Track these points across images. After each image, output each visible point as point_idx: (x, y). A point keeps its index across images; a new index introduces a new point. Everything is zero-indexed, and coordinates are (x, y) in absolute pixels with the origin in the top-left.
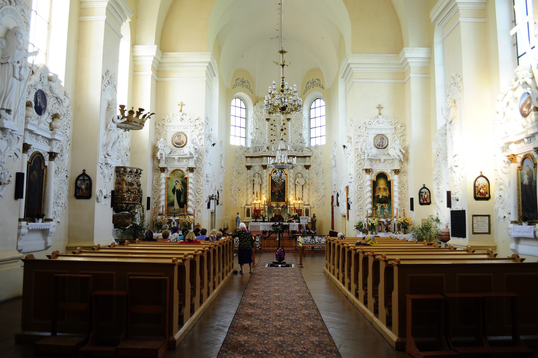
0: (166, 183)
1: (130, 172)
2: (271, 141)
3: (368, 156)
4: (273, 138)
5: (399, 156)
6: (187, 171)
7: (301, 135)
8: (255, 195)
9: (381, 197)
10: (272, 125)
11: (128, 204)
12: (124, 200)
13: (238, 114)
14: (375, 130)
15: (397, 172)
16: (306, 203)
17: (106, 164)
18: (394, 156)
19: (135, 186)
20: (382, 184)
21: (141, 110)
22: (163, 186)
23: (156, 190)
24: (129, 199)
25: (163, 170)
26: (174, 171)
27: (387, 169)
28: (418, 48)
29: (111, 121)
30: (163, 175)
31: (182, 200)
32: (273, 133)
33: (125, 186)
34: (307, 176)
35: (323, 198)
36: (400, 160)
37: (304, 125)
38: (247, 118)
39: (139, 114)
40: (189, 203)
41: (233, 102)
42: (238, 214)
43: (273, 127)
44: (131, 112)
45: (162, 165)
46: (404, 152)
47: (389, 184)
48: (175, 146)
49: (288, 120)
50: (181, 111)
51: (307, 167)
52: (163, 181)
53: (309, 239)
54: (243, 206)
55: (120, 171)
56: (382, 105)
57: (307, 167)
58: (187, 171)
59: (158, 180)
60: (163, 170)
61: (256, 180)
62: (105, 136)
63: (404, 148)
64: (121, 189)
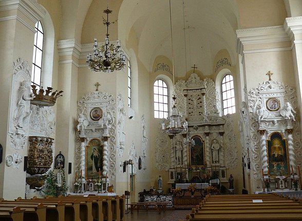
0: (86, 150)
1: (41, 140)
2: (190, 113)
3: (261, 118)
4: (191, 111)
5: (290, 116)
6: (102, 140)
7: (215, 106)
8: (178, 160)
9: (276, 156)
10: (189, 99)
11: (39, 168)
12: (35, 165)
13: (161, 93)
14: (267, 94)
15: (289, 132)
16: (222, 166)
17: (17, 134)
18: (286, 117)
19: (46, 152)
20: (277, 143)
21: (49, 89)
22: (84, 153)
23: (78, 157)
24: (40, 164)
25: (83, 140)
26: (92, 140)
27: (282, 130)
28: (299, 17)
29: (21, 98)
30: (83, 144)
31: (99, 165)
32: (191, 106)
33: (36, 153)
34: (222, 142)
35: (236, 160)
36: (293, 120)
37: (217, 98)
38: (43, 68)
39: (48, 92)
40: (105, 167)
41: (156, 83)
42: (160, 176)
43: (190, 101)
44: (41, 91)
45: (83, 135)
46: (295, 112)
47: (284, 143)
48: (93, 120)
49: (203, 94)
50: (97, 90)
51: (222, 134)
52: (83, 149)
53: (156, 198)
54: (166, 170)
55: (33, 140)
56: (271, 72)
57: (222, 134)
58: (102, 140)
59: (80, 149)
60: (83, 140)
61: (178, 147)
62: (17, 111)
63: (295, 110)
64: (33, 155)
